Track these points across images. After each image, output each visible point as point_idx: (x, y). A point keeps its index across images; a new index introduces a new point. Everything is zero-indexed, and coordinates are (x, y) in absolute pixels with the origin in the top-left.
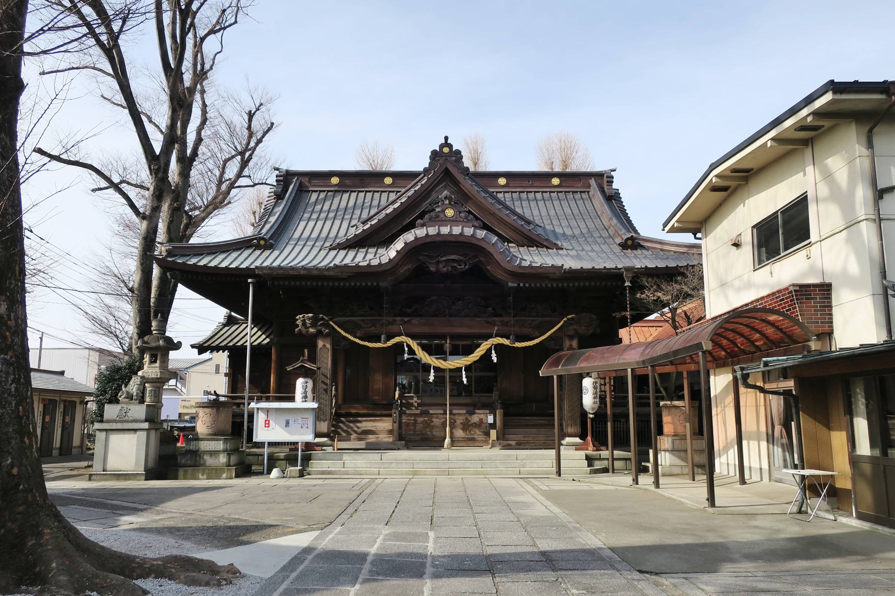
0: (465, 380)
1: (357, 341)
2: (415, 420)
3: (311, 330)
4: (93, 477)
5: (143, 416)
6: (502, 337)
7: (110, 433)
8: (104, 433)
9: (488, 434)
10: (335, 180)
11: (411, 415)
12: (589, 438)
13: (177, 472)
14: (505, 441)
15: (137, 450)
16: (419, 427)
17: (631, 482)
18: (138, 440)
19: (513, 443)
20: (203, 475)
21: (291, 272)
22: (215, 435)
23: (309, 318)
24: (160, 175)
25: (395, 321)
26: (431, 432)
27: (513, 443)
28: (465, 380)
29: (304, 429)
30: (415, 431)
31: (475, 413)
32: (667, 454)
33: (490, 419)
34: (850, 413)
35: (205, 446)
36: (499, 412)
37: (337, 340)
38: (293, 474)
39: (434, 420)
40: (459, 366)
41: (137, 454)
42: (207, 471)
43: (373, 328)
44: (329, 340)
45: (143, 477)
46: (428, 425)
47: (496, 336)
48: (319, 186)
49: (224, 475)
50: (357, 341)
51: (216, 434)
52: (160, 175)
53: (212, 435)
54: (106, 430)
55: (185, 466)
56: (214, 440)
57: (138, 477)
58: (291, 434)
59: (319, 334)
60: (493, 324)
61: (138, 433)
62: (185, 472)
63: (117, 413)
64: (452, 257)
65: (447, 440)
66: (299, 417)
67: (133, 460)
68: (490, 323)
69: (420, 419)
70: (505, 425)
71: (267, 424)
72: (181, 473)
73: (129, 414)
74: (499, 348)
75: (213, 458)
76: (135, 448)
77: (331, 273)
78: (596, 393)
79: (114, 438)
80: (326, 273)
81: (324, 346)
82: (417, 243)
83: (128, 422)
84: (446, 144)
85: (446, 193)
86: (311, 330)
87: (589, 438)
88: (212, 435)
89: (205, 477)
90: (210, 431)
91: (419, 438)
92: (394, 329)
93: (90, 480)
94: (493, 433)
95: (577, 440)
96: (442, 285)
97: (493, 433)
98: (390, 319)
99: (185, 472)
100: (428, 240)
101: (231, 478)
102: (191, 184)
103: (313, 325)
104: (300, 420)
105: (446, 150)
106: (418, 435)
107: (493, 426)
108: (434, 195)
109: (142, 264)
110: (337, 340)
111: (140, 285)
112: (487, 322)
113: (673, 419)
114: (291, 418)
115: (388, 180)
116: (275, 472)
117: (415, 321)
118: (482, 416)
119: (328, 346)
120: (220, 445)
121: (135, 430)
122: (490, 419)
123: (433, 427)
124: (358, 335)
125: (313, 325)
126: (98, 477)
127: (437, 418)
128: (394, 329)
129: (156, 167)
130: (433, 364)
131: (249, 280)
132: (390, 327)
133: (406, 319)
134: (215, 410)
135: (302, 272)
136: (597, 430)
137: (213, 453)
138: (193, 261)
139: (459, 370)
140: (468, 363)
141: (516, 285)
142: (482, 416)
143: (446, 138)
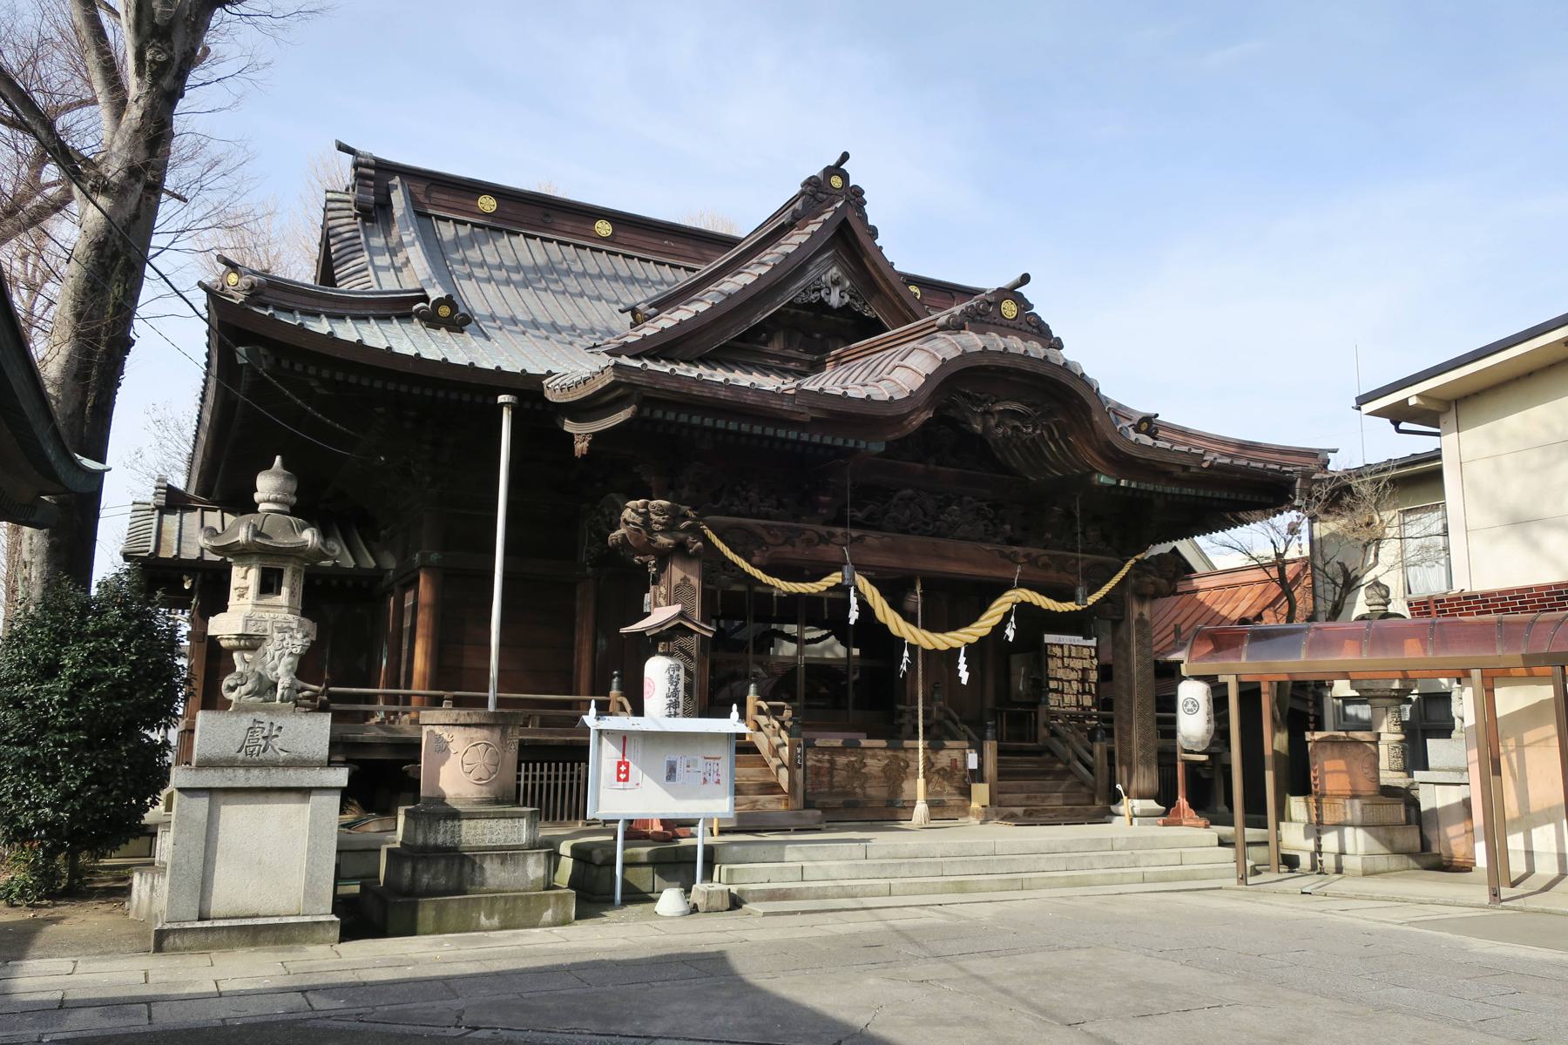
0: (964, 676)
1: (758, 574)
2: (832, 762)
3: (663, 540)
4: (170, 941)
5: (321, 749)
6: (1031, 589)
7: (221, 798)
8: (202, 803)
9: (966, 793)
10: (488, 204)
11: (823, 749)
12: (1182, 801)
13: (413, 909)
14: (999, 809)
15: (312, 851)
16: (840, 777)
17: (1486, 899)
18: (314, 822)
19: (1019, 811)
20: (489, 916)
21: (696, 390)
22: (497, 801)
23: (663, 511)
24: (166, 82)
25: (832, 535)
26: (863, 787)
27: (1019, 811)
28: (964, 676)
29: (711, 785)
30: (831, 786)
31: (943, 747)
32: (1360, 832)
33: (973, 761)
34: (983, 738)
35: (473, 834)
36: (990, 747)
37: (713, 566)
38: (716, 902)
39: (868, 761)
40: (956, 644)
41: (311, 862)
42: (500, 905)
43: (788, 548)
44: (696, 566)
45: (335, 933)
46: (856, 771)
47: (1021, 585)
48: (450, 209)
49: (548, 915)
50: (758, 574)
51: (504, 799)
52: (166, 82)
53: (489, 802)
54: (210, 791)
55: (431, 892)
56: (488, 816)
57: (320, 934)
58: (677, 796)
59: (680, 551)
60: (1013, 560)
61: (314, 798)
62: (440, 910)
63: (240, 737)
64: (1015, 406)
65: (921, 809)
66: (698, 755)
67: (298, 882)
68: (1007, 557)
69: (842, 760)
70: (1002, 774)
71: (623, 773)
72: (427, 911)
73: (277, 743)
74: (1023, 609)
75: (510, 866)
76: (303, 843)
77: (786, 406)
78: (675, 693)
79: (237, 818)
80: (775, 403)
81: (685, 579)
82: (1042, 370)
83: (275, 765)
84: (836, 170)
85: (834, 272)
86: (663, 540)
87: (1182, 801)
88: (489, 802)
89: (496, 921)
90: (485, 792)
91: (840, 801)
92: (830, 552)
93: (159, 948)
94: (981, 792)
95: (1152, 805)
96: (921, 466)
97: (981, 792)
98: (823, 530)
99: (440, 910)
100: (985, 362)
101: (565, 922)
102: (176, 132)
103: (669, 529)
104: (701, 761)
105: (836, 182)
106: (838, 794)
107: (978, 775)
108: (812, 273)
109: (78, 316)
110: (713, 566)
111: (65, 371)
112: (1002, 555)
113: (1347, 764)
114: (679, 757)
115: (603, 228)
116: (670, 900)
117: (872, 538)
118: (956, 754)
119: (695, 581)
120: (518, 831)
121: (305, 792)
122: (973, 761)
123: (867, 777)
124: (756, 559)
125: (669, 529)
126: (188, 940)
127: (873, 757)
128: (830, 552)
129: (162, 57)
130: (909, 639)
131: (502, 399)
132: (822, 547)
133: (855, 534)
134: (497, 735)
135: (722, 394)
136: (1200, 789)
137: (508, 854)
138: (294, 320)
139: (954, 652)
140: (973, 640)
141: (1113, 482)
142: (956, 754)
143: (845, 157)
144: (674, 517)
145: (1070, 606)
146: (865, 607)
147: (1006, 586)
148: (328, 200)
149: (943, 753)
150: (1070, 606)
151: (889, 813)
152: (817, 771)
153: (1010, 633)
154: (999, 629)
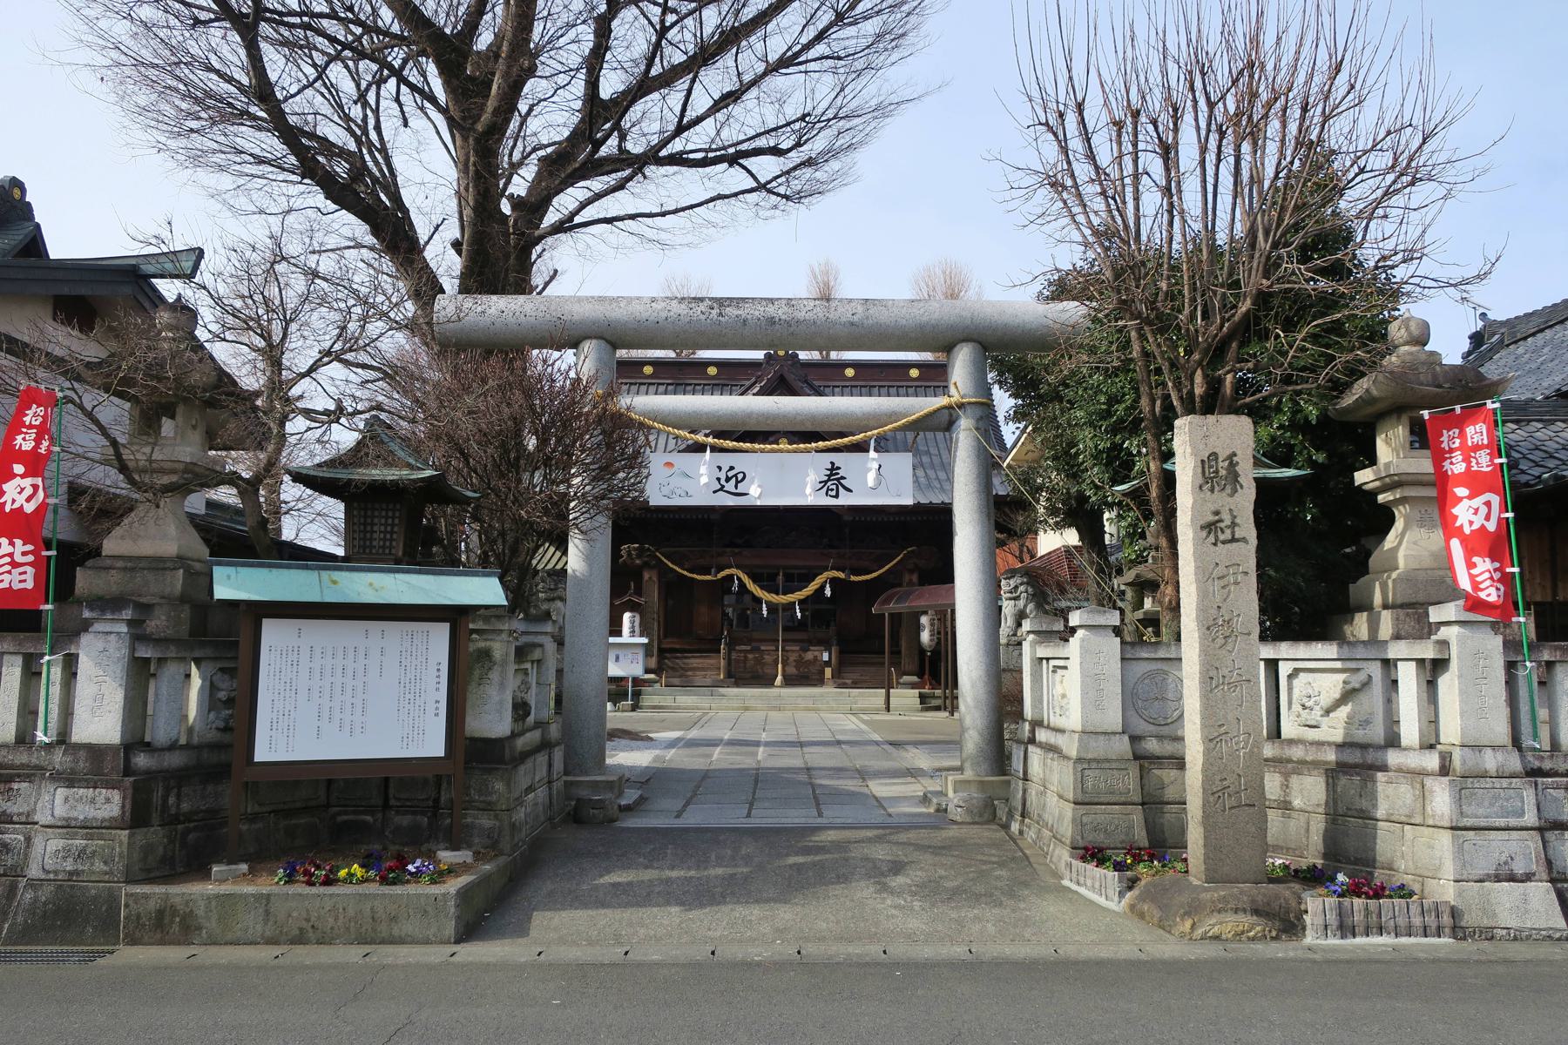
16: (750, 663)
33: (826, 657)
59: (646, 565)
69: (750, 656)
74: (833, 581)
94: (828, 672)
95: (915, 679)
103: (639, 556)
107: (828, 664)
110: (664, 572)
122: (826, 657)
125: (639, 556)
144: (641, 551)
145: (708, 578)
146: (742, 585)
147: (826, 569)
148: (236, 658)
149: (1338, 736)
150: (708, 578)
151: (768, 682)
152: (737, 661)
153: (828, 592)
154: (822, 587)
